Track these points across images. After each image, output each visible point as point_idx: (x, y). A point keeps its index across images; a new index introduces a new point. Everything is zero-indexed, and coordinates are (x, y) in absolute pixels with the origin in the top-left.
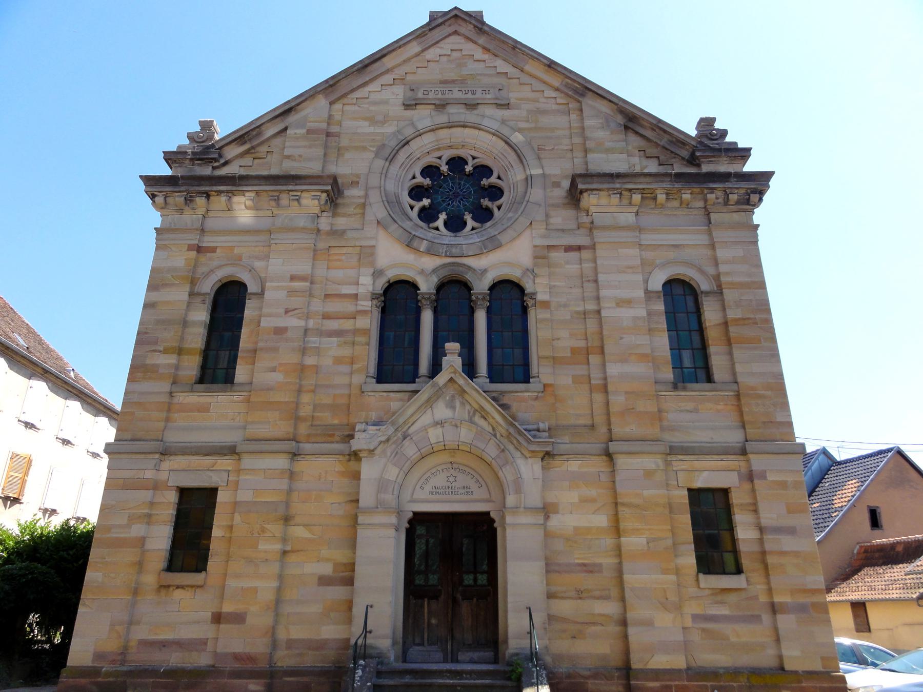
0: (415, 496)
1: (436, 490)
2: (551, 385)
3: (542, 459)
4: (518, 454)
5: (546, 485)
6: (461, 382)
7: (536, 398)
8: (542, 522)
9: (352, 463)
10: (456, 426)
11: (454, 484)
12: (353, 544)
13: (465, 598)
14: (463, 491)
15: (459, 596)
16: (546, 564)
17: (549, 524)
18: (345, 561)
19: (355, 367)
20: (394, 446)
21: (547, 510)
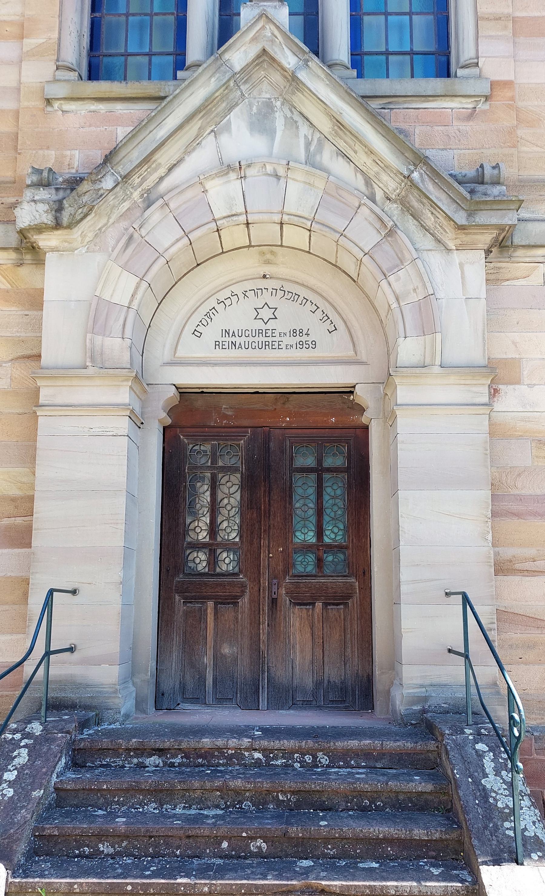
0: (181, 353)
1: (229, 339)
2: (508, 84)
3: (488, 252)
4: (427, 242)
5: (494, 319)
6: (289, 59)
7: (472, 115)
8: (485, 399)
9: (24, 271)
10: (277, 177)
11: (271, 325)
12: (29, 454)
13: (299, 601)
14: (293, 341)
15: (285, 599)
16: (494, 497)
17: (498, 406)
18: (15, 492)
19: (30, 43)
20: (124, 224)
21: (496, 374)
